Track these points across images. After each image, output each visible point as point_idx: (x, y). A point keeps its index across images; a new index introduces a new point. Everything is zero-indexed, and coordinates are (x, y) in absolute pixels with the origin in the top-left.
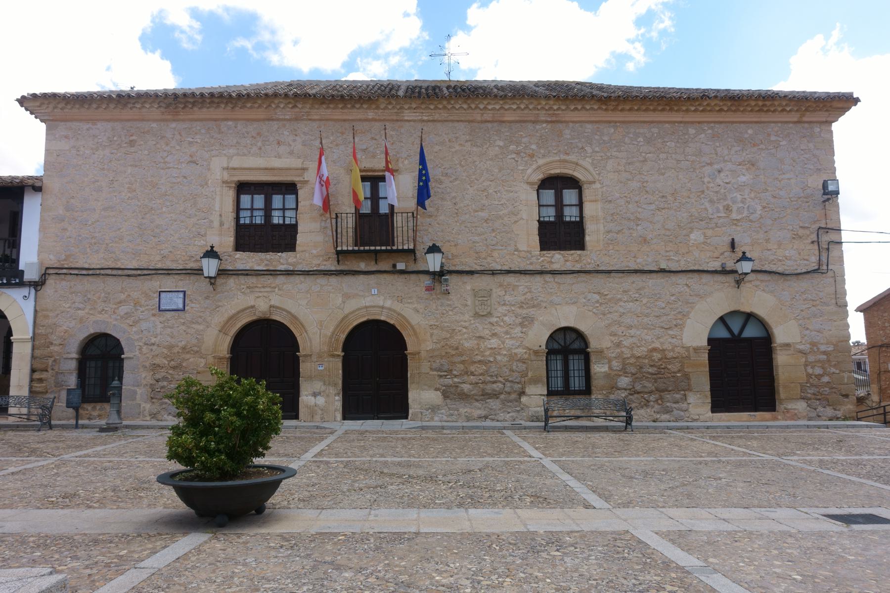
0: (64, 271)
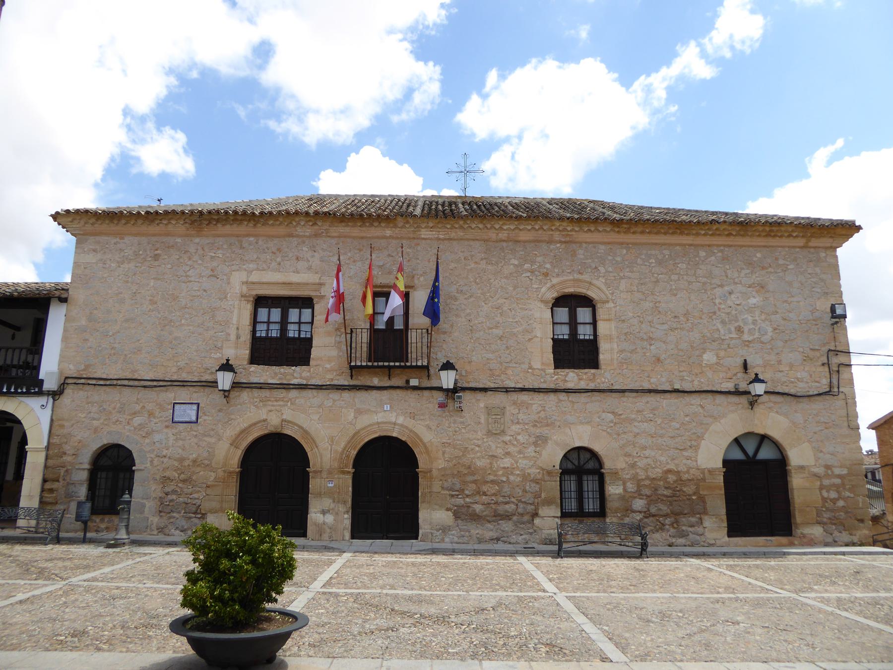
0: (82, 381)
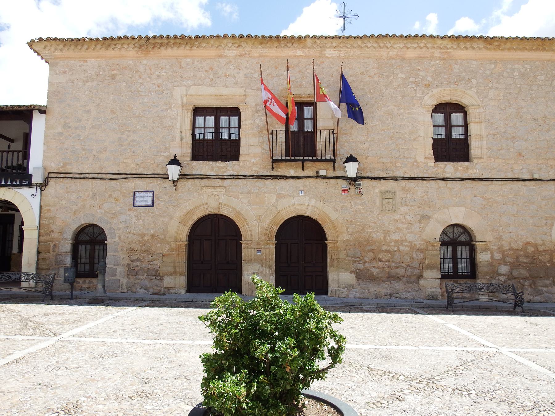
0: (62, 175)
